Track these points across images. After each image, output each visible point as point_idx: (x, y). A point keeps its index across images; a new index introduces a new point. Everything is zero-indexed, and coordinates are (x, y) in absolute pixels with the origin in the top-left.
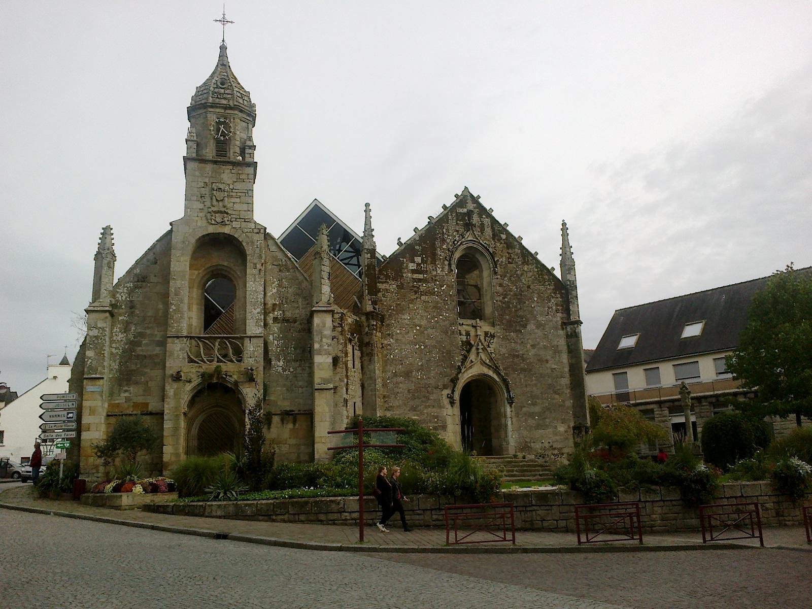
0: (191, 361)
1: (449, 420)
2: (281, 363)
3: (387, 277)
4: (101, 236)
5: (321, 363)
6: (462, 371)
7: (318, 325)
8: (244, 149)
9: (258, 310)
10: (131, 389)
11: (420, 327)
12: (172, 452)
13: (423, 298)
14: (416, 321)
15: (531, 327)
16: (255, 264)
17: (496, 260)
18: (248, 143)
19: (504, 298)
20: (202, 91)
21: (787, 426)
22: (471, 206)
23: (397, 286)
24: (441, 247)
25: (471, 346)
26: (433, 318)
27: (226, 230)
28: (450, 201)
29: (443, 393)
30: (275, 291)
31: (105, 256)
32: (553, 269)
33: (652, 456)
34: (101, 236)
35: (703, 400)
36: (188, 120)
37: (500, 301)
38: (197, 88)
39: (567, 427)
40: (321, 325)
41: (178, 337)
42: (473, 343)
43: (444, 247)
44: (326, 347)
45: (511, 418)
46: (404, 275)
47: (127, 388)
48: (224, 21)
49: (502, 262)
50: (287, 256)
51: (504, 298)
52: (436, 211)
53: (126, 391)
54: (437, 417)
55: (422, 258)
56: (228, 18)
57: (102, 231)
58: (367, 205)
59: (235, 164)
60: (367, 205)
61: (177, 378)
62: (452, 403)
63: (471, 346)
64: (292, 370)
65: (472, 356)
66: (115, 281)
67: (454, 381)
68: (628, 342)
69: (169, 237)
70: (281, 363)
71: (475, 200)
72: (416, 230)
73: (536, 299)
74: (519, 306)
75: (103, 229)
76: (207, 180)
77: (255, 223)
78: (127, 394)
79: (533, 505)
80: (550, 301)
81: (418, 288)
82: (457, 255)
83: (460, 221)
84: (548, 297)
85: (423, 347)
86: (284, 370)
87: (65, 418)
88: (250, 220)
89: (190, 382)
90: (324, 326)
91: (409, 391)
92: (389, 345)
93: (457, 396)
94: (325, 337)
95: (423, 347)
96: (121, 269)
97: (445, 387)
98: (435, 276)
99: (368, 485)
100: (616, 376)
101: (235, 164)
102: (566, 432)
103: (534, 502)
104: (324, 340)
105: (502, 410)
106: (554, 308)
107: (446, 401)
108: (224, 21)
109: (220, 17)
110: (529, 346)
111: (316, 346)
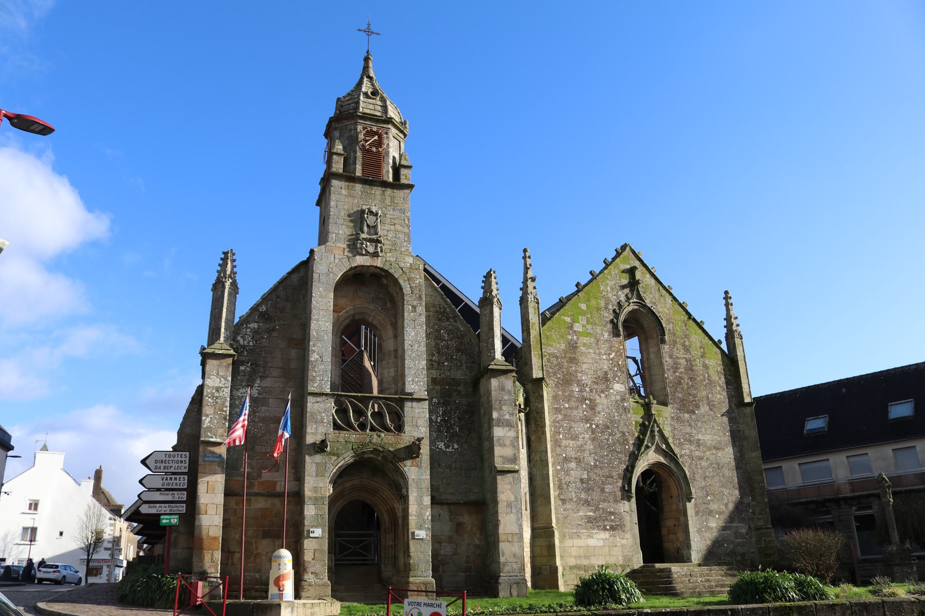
1: (627, 518)
4: (221, 262)
12: (316, 547)
14: (585, 394)
27: (378, 263)
31: (222, 287)
32: (720, 341)
33: (627, 575)
34: (221, 262)
35: (842, 503)
36: (329, 126)
38: (339, 99)
48: (369, 32)
50: (446, 302)
56: (372, 29)
57: (223, 256)
59: (385, 184)
61: (320, 447)
66: (237, 320)
69: (302, 273)
75: (224, 253)
82: (622, 318)
91: (582, 480)
96: (243, 308)
100: (303, 594)
101: (385, 184)
108: (369, 32)
109: (364, 27)
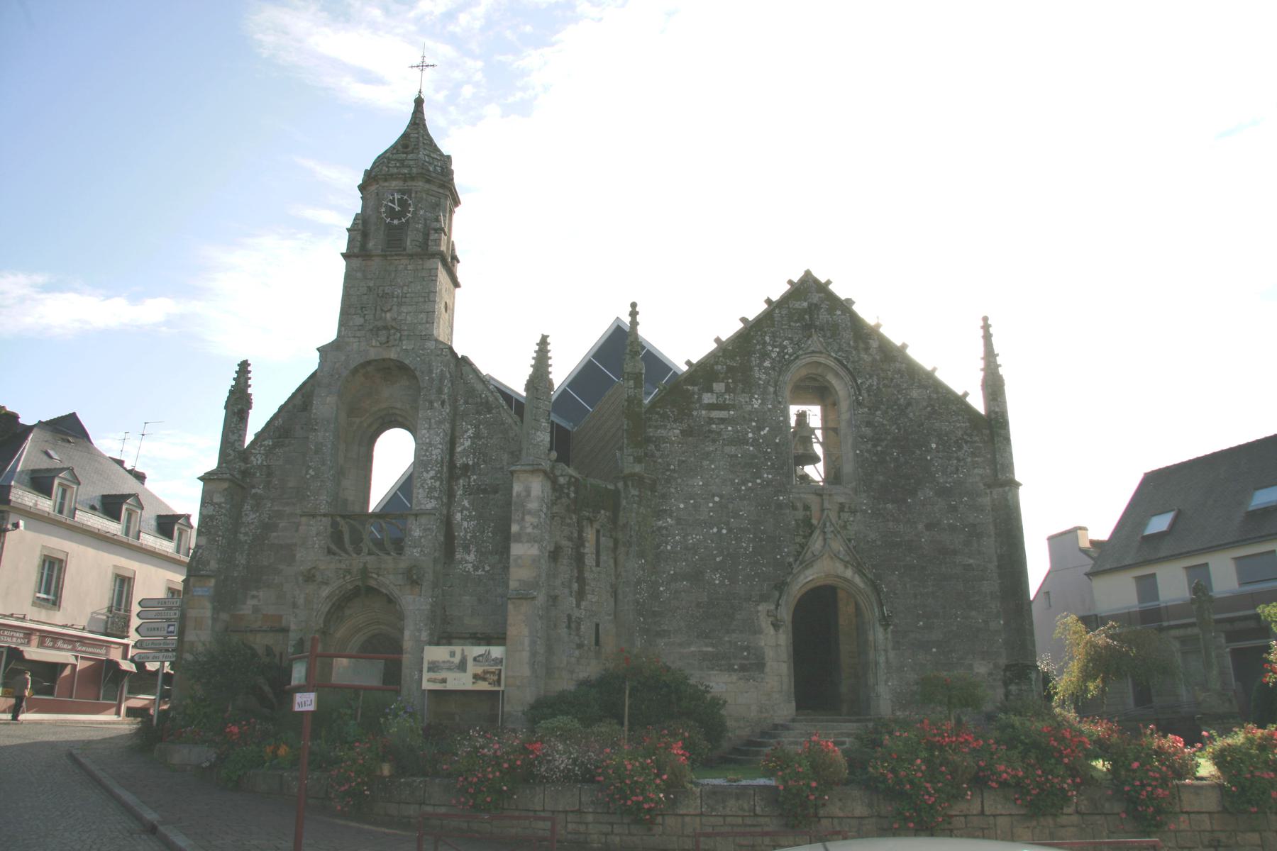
0: (330, 552)
1: (769, 654)
2: (471, 557)
3: (664, 417)
5: (519, 557)
6: (795, 571)
7: (518, 495)
8: (428, 235)
9: (432, 473)
10: (261, 594)
11: (721, 497)
13: (728, 449)
15: (927, 493)
16: (431, 403)
17: (859, 381)
18: (435, 225)
19: (875, 446)
20: (382, 160)
21: (1065, 676)
22: (815, 298)
23: (682, 432)
24: (760, 365)
25: (812, 528)
26: (744, 482)
28: (778, 291)
29: (760, 608)
30: (468, 443)
31: (239, 402)
37: (868, 451)
39: (991, 666)
40: (524, 494)
41: (314, 516)
42: (814, 521)
43: (767, 364)
44: (529, 530)
45: (886, 651)
46: (695, 413)
47: (255, 593)
49: (871, 385)
51: (875, 446)
52: (755, 309)
53: (253, 597)
54: (747, 648)
55: (727, 386)
58: (634, 305)
60: (634, 305)
61: (309, 577)
62: (776, 626)
63: (812, 528)
64: (487, 568)
65: (817, 544)
67: (781, 586)
68: (1159, 524)
70: (471, 557)
71: (823, 288)
72: (718, 340)
73: (934, 446)
74: (902, 459)
76: (371, 284)
77: (436, 340)
78: (255, 602)
79: (756, 815)
80: (960, 448)
81: (719, 433)
83: (796, 322)
84: (956, 442)
85: (724, 531)
86: (476, 568)
87: (164, 633)
88: (429, 337)
89: (327, 584)
90: (529, 495)
92: (666, 528)
93: (786, 614)
94: (530, 513)
95: (724, 531)
96: (257, 421)
97: (764, 598)
98: (750, 413)
99: (1189, 742)
102: (990, 674)
103: (758, 809)
104: (528, 518)
105: (871, 638)
106: (969, 460)
107: (765, 624)
110: (920, 526)
111: (515, 528)
